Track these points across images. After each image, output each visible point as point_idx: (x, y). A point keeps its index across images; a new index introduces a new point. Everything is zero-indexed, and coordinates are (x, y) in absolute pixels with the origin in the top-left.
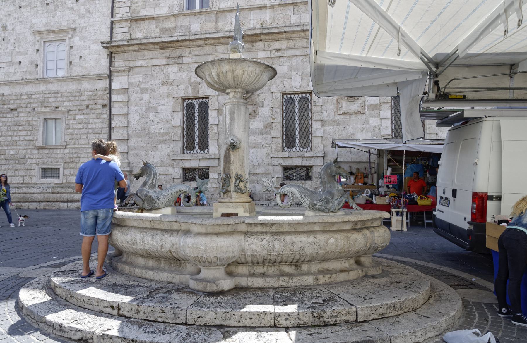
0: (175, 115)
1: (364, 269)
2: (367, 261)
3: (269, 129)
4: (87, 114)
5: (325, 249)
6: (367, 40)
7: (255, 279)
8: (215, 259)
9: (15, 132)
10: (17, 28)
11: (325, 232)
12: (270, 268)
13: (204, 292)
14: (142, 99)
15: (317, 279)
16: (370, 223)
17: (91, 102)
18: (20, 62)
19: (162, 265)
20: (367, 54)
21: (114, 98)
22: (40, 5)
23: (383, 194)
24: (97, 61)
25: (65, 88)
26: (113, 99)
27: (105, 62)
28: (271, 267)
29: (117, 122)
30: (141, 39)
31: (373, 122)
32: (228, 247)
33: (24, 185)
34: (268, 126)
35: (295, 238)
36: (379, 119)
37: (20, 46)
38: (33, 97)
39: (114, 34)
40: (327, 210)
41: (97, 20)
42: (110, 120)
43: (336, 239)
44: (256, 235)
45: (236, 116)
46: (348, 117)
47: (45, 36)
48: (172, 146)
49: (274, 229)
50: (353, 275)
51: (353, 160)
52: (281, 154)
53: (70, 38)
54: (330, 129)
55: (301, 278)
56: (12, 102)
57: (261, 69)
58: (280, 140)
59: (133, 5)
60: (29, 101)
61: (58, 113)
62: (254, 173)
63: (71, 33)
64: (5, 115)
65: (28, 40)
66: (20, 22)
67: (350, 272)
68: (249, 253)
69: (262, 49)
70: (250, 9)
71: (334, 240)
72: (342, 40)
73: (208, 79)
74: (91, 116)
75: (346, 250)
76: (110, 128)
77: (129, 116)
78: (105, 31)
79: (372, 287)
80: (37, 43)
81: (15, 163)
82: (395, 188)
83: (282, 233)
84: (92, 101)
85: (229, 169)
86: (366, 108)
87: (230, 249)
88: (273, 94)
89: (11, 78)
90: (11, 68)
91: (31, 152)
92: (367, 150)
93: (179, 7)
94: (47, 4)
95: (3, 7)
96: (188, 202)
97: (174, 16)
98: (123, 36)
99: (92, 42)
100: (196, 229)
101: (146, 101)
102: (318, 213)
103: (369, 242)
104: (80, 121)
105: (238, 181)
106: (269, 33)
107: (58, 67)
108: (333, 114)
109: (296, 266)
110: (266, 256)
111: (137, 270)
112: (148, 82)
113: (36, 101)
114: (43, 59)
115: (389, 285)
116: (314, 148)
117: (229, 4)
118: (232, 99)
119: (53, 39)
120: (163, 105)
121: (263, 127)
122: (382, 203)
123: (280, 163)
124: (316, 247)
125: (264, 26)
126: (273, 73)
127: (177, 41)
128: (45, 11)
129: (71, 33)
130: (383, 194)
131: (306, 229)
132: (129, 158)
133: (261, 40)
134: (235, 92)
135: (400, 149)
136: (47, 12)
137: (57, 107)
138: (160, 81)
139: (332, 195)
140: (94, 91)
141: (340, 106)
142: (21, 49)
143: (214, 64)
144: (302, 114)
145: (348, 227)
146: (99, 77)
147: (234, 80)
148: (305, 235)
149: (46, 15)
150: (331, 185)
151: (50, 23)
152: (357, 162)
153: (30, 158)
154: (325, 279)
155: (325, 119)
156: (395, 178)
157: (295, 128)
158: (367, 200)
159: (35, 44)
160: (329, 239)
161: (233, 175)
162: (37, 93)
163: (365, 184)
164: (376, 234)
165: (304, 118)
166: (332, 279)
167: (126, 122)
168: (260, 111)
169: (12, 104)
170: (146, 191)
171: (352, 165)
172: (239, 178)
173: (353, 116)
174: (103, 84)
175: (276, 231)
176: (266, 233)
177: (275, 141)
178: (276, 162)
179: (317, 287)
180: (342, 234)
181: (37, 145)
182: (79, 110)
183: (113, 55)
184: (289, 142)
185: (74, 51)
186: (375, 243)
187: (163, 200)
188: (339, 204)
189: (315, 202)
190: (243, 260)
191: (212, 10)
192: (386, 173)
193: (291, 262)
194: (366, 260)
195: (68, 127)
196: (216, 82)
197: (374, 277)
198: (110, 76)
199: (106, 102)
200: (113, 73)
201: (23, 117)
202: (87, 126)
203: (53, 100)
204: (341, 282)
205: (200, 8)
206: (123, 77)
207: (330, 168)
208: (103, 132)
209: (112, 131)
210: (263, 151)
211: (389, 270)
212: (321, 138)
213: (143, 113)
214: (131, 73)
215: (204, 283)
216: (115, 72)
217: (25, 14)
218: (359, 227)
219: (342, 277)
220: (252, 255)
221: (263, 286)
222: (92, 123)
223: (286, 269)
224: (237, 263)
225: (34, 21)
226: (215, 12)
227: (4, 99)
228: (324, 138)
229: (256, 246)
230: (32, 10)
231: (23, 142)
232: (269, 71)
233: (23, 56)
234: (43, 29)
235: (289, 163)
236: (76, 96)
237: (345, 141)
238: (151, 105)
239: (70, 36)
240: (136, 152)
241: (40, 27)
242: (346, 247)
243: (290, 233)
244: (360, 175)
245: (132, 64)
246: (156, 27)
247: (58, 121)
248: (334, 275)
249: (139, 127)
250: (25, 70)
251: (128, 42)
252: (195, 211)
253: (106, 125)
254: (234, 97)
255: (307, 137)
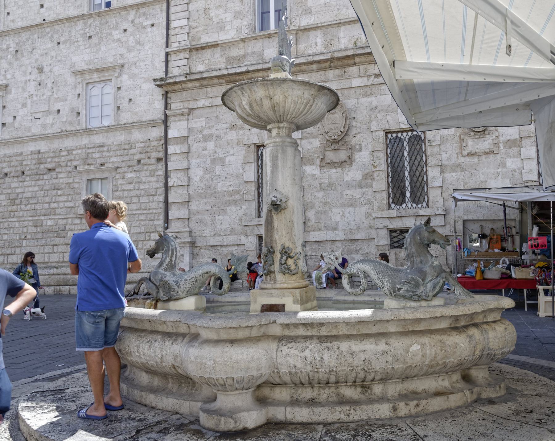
0: (247, 167)
1: (475, 390)
2: (480, 376)
3: (369, 181)
4: (138, 171)
5: (405, 362)
6: (464, 39)
7: (297, 409)
8: (230, 381)
9: (54, 198)
10: (56, 69)
11: (405, 334)
12: (322, 392)
13: (217, 432)
14: (206, 149)
15: (395, 409)
16: (481, 317)
17: (143, 156)
18: (59, 111)
19: (170, 385)
20: (471, 61)
21: (171, 149)
22: (81, 39)
23: (529, 263)
24: (148, 103)
25: (112, 139)
26: (170, 152)
27: (159, 104)
28: (324, 389)
29: (175, 180)
30: (202, 72)
31: (512, 163)
32: (249, 361)
33: (64, 264)
34: (368, 176)
35: (356, 346)
36: (519, 159)
37: (58, 90)
38: (74, 152)
39: (170, 69)
40: (416, 297)
41: (149, 52)
42: (167, 177)
43: (423, 345)
44: (295, 341)
45: (280, 163)
46: (476, 160)
47: (87, 76)
48: (244, 207)
49: (324, 332)
50: (455, 400)
51: (485, 218)
52: (387, 214)
53: (117, 77)
54: (452, 177)
55: (370, 407)
56: (49, 160)
57: (312, 92)
58: (385, 195)
59: (192, 31)
60: (69, 157)
61: (103, 171)
62: (352, 240)
63: (118, 70)
64: (41, 177)
65: (68, 83)
66: (59, 61)
67: (451, 396)
68: (284, 370)
69: (356, 75)
70: (340, 24)
71: (418, 347)
72: (426, 42)
73: (239, 111)
74: (143, 174)
75: (440, 362)
76: (167, 188)
77: (190, 171)
78: (158, 66)
79: (484, 422)
80: (78, 86)
81: (54, 237)
82: (544, 255)
83: (336, 337)
84: (144, 154)
85: (272, 240)
86: (501, 145)
87: (253, 365)
88: (374, 133)
89: (49, 131)
90: (48, 118)
91: (72, 222)
92: (501, 203)
93: (249, 29)
94: (90, 37)
95: (39, 44)
96: (220, 288)
97: (243, 40)
98: (180, 71)
99: (143, 80)
100: (205, 334)
101: (211, 152)
102: (403, 303)
103: (479, 348)
104: (130, 181)
105: (285, 257)
106: (364, 54)
107: (104, 114)
108: (455, 155)
109: (363, 387)
110: (311, 374)
111: (136, 391)
112: (213, 126)
113: (77, 158)
114: (86, 105)
115: (513, 418)
116: (430, 204)
117: (313, 20)
118: (274, 138)
119: (97, 80)
120: (231, 155)
121: (361, 178)
122: (524, 277)
123: (385, 224)
124: (390, 359)
125: (358, 45)
126: (333, 99)
127: (248, 72)
128: (87, 46)
129: (118, 70)
130: (529, 263)
131: (375, 330)
132: (190, 226)
133: (355, 64)
134: (279, 128)
135: (545, 199)
136: (89, 47)
137: (102, 165)
138: (228, 125)
139: (423, 275)
140: (146, 142)
141: (464, 144)
142: (60, 95)
143: (242, 88)
144: (413, 158)
145: (444, 325)
146: (152, 124)
147: (274, 110)
148: (372, 340)
149: (89, 50)
150: (422, 258)
151: (94, 59)
152: (490, 220)
153: (71, 230)
154: (408, 408)
155: (445, 163)
156: (542, 241)
157: (405, 177)
158: (503, 274)
159: (76, 87)
160: (411, 346)
161: (278, 248)
162: (78, 147)
163: (503, 249)
164: (491, 334)
165: (416, 163)
166: (421, 408)
167: (186, 179)
168: (357, 156)
169: (50, 163)
170: (162, 274)
171: (484, 224)
172: (286, 253)
173: (484, 157)
174: (157, 132)
175: (327, 334)
176: (311, 337)
177: (378, 195)
178: (380, 224)
179: (394, 422)
180: (433, 336)
181: (79, 213)
182: (129, 167)
183: (169, 95)
184: (397, 196)
185: (122, 93)
186: (489, 349)
187: (185, 286)
188: (434, 288)
189: (397, 286)
190: (278, 380)
191: (291, 29)
192: (532, 234)
193: (355, 382)
194: (479, 374)
195: (116, 189)
196: (250, 115)
197: (491, 402)
198: (165, 122)
199: (161, 155)
200: (169, 118)
201: (63, 178)
202: (139, 186)
203: (97, 155)
204: (436, 412)
205: (276, 28)
206: (181, 123)
207: (420, 234)
208: (158, 193)
209: (169, 191)
210: (363, 210)
211: (519, 388)
212: (440, 189)
213: (208, 166)
214: (191, 117)
215: (216, 417)
216: (171, 116)
217: (65, 51)
218: (462, 323)
219: (437, 404)
220: (290, 373)
221: (310, 421)
222: (145, 183)
223: (348, 392)
224: (271, 384)
225: (74, 59)
226: (295, 32)
227: (40, 157)
228: (444, 189)
229: (294, 358)
230: (72, 46)
231: (63, 210)
232: (325, 94)
233: (62, 103)
234: (86, 67)
235: (398, 224)
236: (125, 149)
237: (468, 193)
238: (217, 155)
239: (117, 74)
240: (199, 217)
241: (82, 66)
242: (439, 358)
243: (348, 337)
244: (495, 237)
245: (192, 105)
246: (221, 56)
247: (104, 181)
248: (424, 402)
249: (202, 185)
250: (64, 120)
251: (186, 77)
252: (238, 299)
253: (162, 184)
254: (278, 135)
255: (421, 189)
